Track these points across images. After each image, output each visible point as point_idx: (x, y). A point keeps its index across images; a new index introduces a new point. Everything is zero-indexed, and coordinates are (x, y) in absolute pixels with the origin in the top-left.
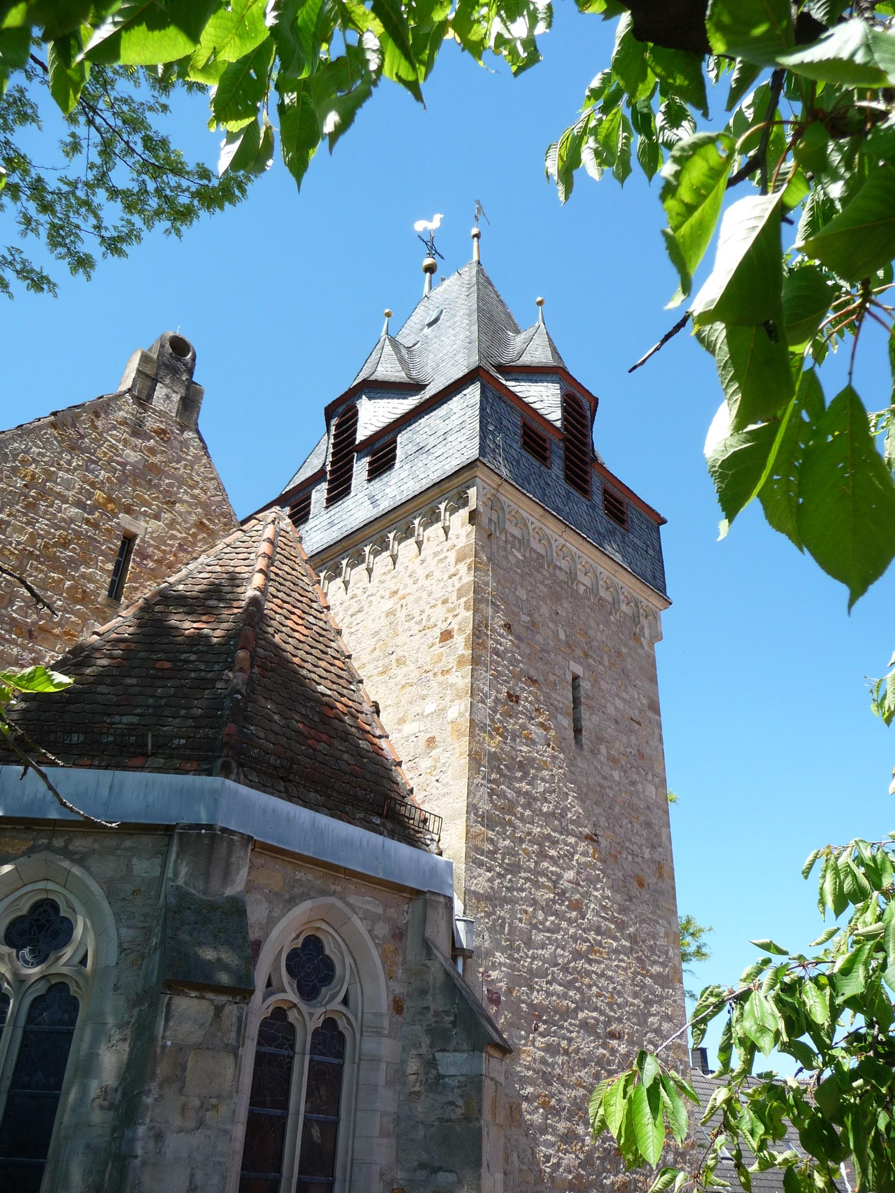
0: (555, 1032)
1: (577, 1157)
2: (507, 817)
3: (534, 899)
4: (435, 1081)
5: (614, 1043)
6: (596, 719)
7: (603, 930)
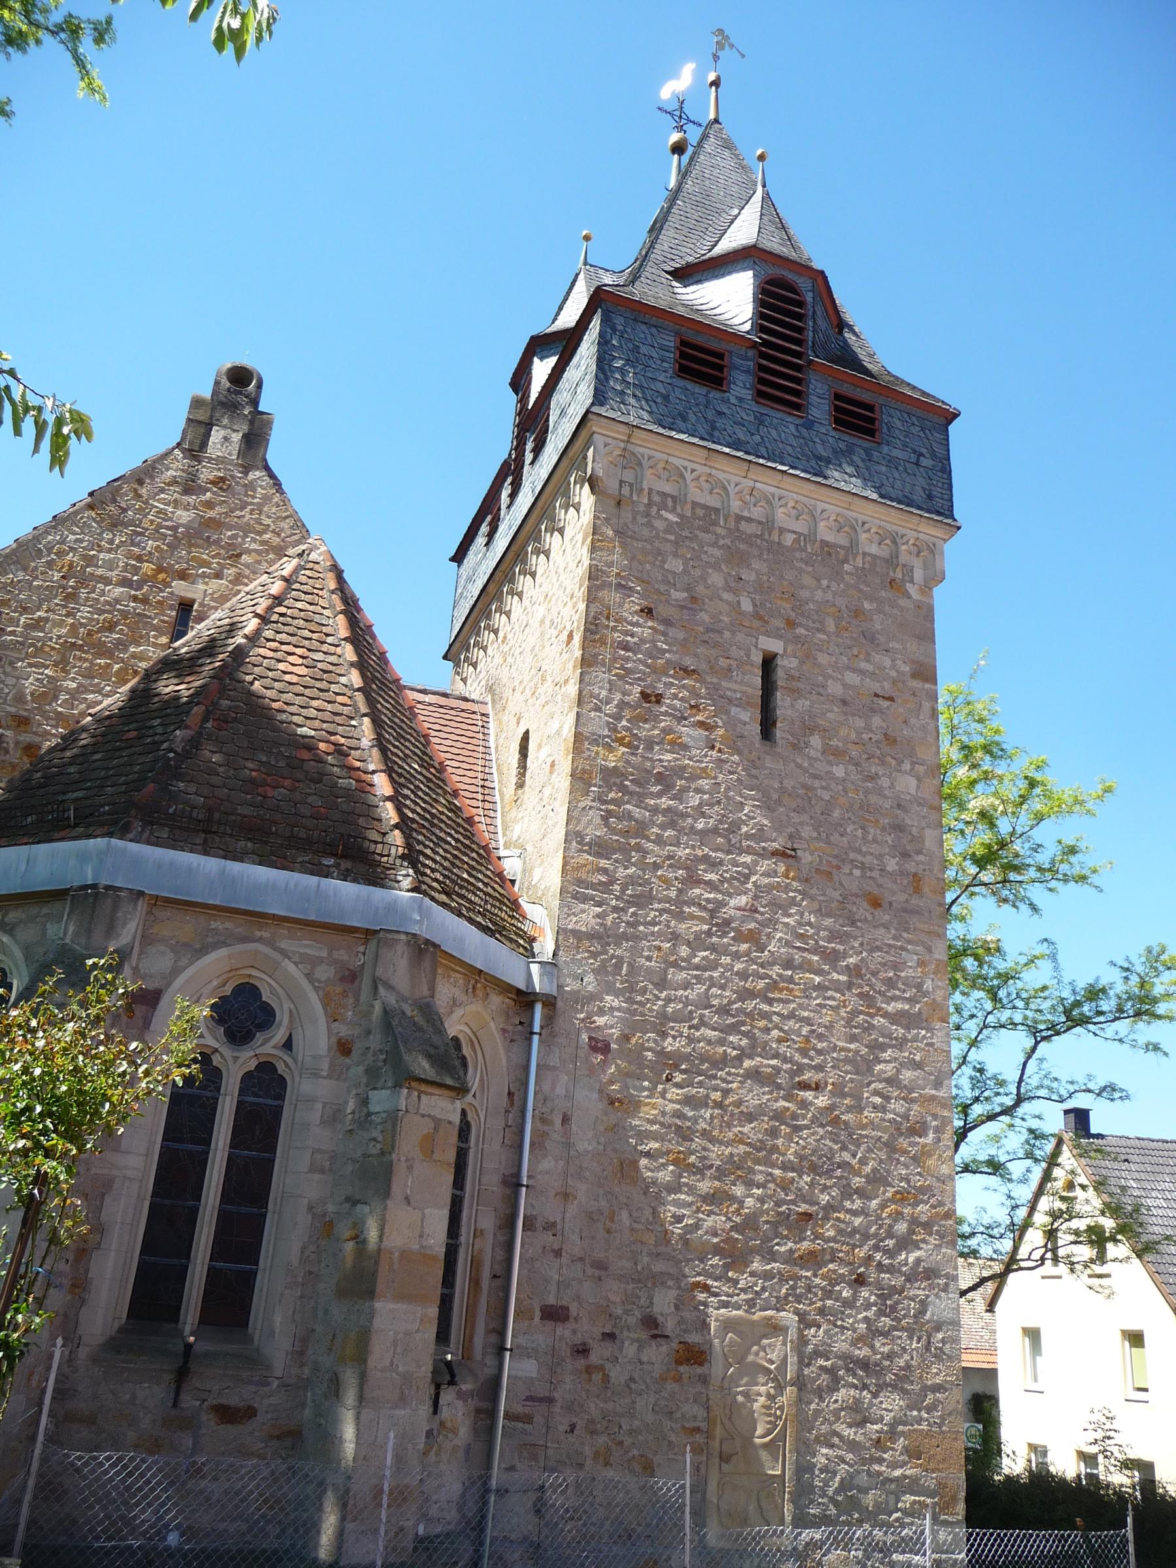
0: (700, 1082)
1: (729, 1219)
2: (633, 842)
3: (672, 933)
4: (364, 1119)
5: (809, 1095)
6: (803, 704)
7: (796, 963)
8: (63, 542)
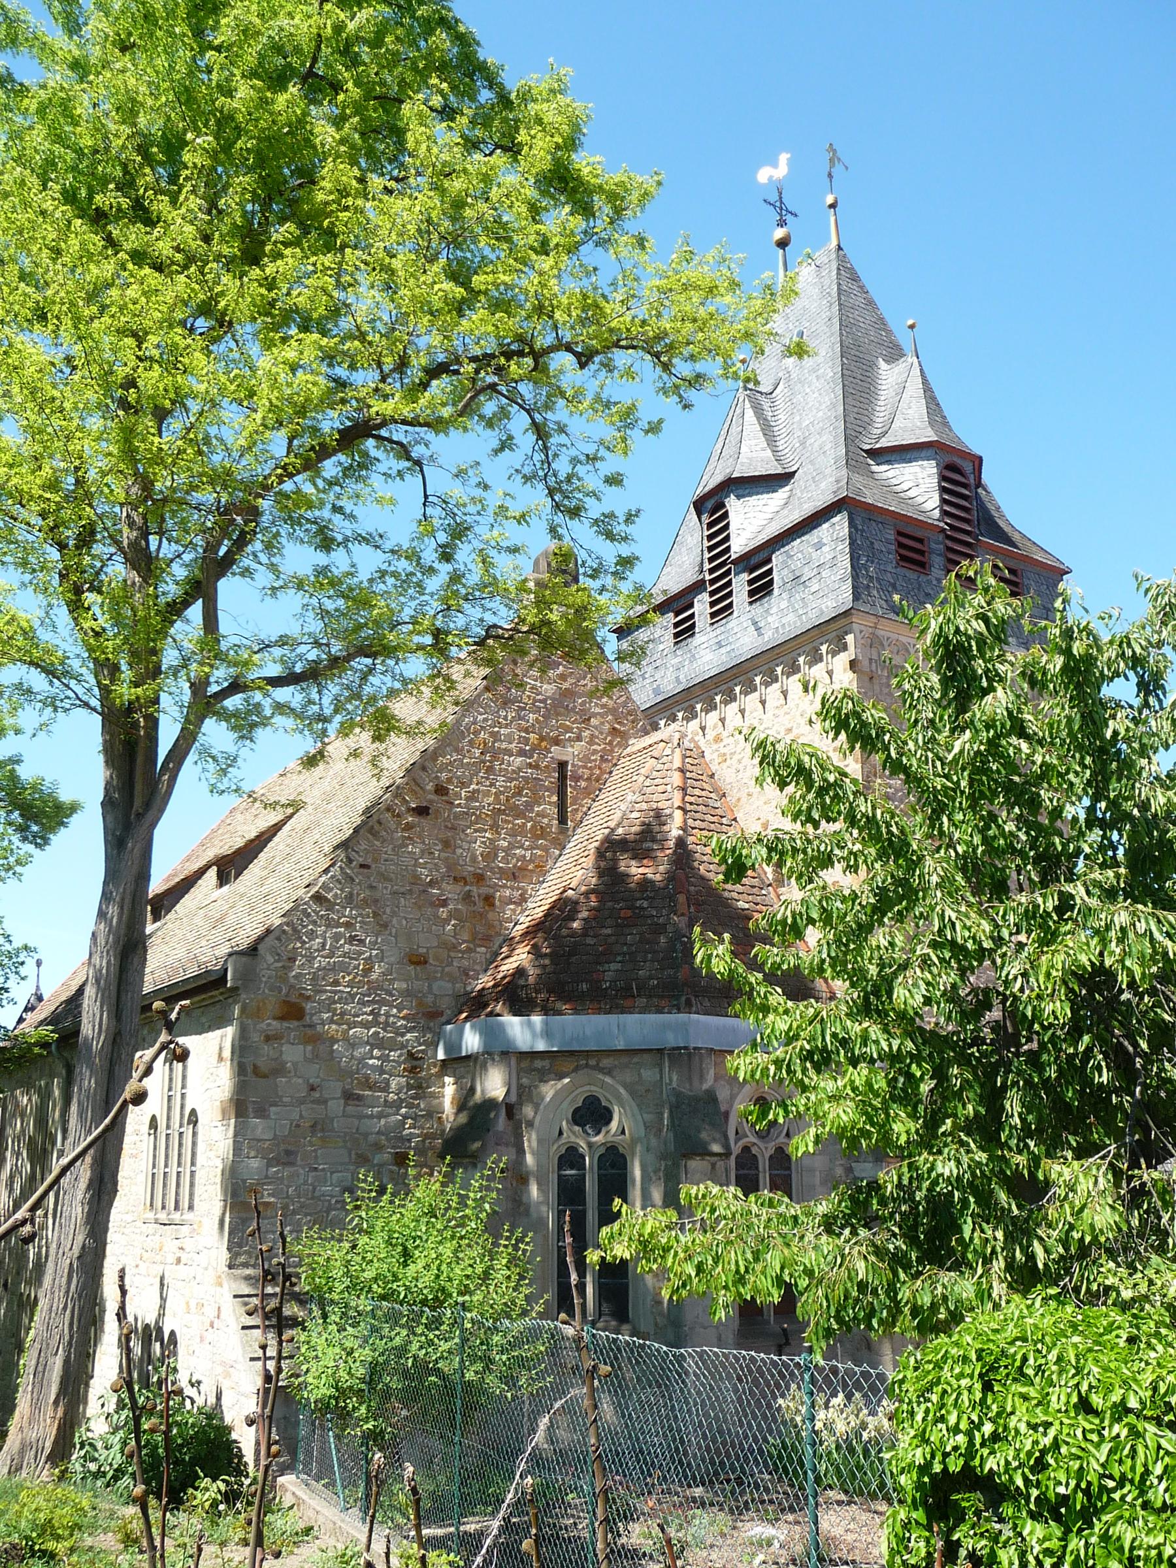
8: (475, 723)
